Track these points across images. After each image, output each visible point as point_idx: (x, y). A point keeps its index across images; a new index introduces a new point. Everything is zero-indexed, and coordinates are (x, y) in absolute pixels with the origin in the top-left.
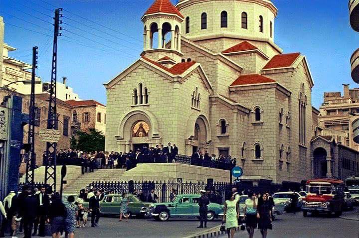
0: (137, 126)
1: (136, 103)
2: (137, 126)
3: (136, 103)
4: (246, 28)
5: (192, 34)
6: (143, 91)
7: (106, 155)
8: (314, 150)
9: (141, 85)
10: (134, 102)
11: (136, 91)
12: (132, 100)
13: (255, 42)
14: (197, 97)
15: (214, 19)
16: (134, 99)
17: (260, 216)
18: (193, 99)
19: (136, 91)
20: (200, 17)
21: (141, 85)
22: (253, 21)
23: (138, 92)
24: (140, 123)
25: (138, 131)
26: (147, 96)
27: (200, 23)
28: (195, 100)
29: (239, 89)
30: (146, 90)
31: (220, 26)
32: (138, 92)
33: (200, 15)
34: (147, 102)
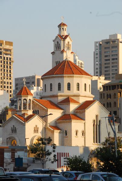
0: (13, 142)
1: (12, 133)
2: (13, 142)
3: (12, 133)
4: (70, 90)
5: (63, 92)
6: (15, 128)
7: (100, 85)
8: (82, 179)
9: (14, 126)
10: (12, 132)
11: (12, 128)
12: (11, 131)
13: (74, 97)
14: (37, 129)
15: (56, 87)
16: (12, 131)
17: (103, 162)
18: (34, 130)
19: (12, 128)
20: (58, 85)
21: (14, 126)
22: (82, 87)
23: (13, 128)
24: (13, 141)
25: (13, 144)
26: (16, 130)
27: (58, 87)
28: (36, 130)
29: (60, 122)
30: (15, 128)
31: (58, 90)
32: (13, 128)
33: (58, 83)
34: (16, 132)
